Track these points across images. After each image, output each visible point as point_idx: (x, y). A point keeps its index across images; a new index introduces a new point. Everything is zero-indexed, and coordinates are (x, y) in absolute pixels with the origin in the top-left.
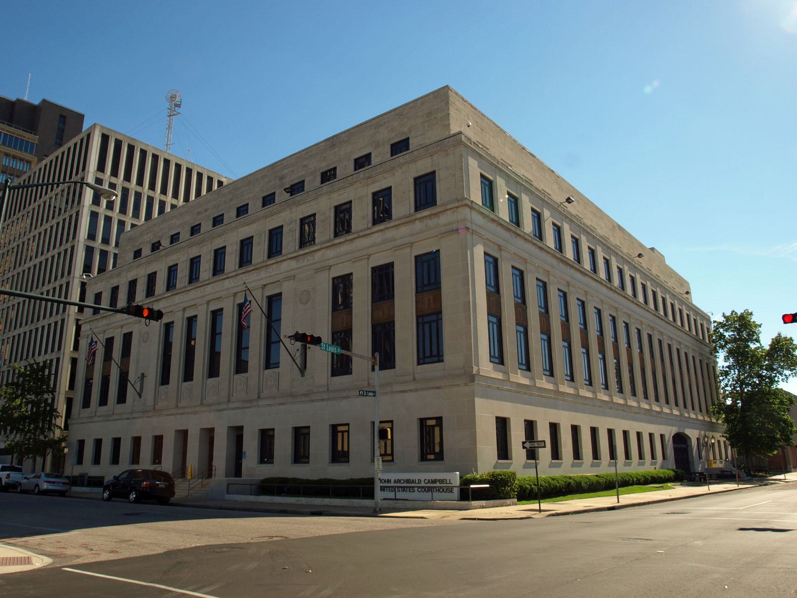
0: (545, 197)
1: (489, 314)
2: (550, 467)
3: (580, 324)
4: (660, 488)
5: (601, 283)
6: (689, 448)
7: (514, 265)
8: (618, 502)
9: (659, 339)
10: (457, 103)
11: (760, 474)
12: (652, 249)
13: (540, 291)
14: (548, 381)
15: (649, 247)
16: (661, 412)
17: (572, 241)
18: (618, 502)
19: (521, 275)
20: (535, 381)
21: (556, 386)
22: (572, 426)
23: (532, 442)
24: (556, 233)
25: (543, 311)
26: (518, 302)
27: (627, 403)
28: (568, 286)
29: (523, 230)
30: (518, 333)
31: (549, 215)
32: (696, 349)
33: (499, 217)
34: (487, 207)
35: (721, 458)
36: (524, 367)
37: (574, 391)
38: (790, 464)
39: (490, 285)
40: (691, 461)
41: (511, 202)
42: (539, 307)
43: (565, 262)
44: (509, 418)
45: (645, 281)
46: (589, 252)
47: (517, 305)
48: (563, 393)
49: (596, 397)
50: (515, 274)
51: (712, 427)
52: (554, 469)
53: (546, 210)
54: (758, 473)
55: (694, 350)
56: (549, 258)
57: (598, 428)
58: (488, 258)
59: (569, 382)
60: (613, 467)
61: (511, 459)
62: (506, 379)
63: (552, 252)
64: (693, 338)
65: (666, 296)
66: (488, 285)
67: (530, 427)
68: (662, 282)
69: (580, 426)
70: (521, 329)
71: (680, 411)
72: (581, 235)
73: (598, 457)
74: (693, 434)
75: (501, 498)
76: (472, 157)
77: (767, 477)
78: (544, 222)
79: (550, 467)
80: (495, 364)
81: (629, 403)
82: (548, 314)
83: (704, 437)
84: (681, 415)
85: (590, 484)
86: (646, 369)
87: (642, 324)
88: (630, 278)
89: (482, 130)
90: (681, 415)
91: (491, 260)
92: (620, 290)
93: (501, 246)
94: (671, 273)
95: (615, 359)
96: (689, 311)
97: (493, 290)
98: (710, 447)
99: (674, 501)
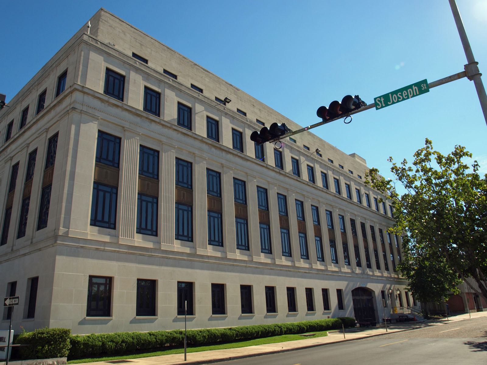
0: (135, 63)
1: (281, 228)
2: (306, 315)
3: (341, 229)
4: (312, 336)
5: (390, 220)
6: (373, 299)
7: (297, 199)
8: (185, 360)
9: (379, 229)
10: (110, 22)
11: (436, 316)
12: (353, 155)
13: (299, 207)
14: (335, 266)
15: (348, 153)
16: (382, 276)
17: (356, 191)
18: (185, 360)
19: (300, 204)
20: (227, 253)
21: (326, 267)
22: (214, 286)
23: (13, 298)
24: (358, 193)
25: (330, 227)
26: (330, 228)
27: (295, 265)
28: (223, 167)
29: (302, 178)
30: (317, 241)
31: (305, 160)
32: (383, 223)
33: (318, 186)
34: (296, 174)
35: (408, 304)
36: (335, 262)
37: (248, 258)
38: (467, 307)
39: (299, 217)
40: (375, 309)
41: (309, 169)
42: (341, 229)
43: (353, 203)
44: (276, 287)
45: (359, 187)
46: (374, 200)
47: (329, 230)
48: (299, 268)
49: (327, 269)
50: (313, 209)
51: (398, 281)
52: (269, 320)
53: (247, 129)
54: (434, 316)
55: (381, 224)
56: (273, 174)
57: (114, 277)
58: (297, 202)
59: (347, 266)
60: (183, 321)
61: (315, 311)
62: (293, 265)
63: (321, 189)
64: (382, 216)
65: (350, 183)
66: (260, 205)
67: (309, 292)
68: (346, 173)
69: (313, 288)
70: (318, 239)
71: (352, 269)
72: (315, 164)
73: (330, 309)
74: (376, 288)
75: (38, 358)
76: (133, 71)
77: (439, 319)
78: (301, 164)
79: (287, 316)
80: (320, 262)
81: (297, 265)
82: (268, 210)
83: (389, 290)
84: (353, 272)
85: (251, 333)
86: (322, 238)
87: (319, 202)
88: (389, 207)
89: (141, 45)
90: (363, 273)
91: (328, 213)
92: (349, 200)
93: (288, 188)
94: (365, 170)
95: (391, 254)
96: (377, 195)
97: (330, 227)
98: (397, 297)
99: (307, 349)
